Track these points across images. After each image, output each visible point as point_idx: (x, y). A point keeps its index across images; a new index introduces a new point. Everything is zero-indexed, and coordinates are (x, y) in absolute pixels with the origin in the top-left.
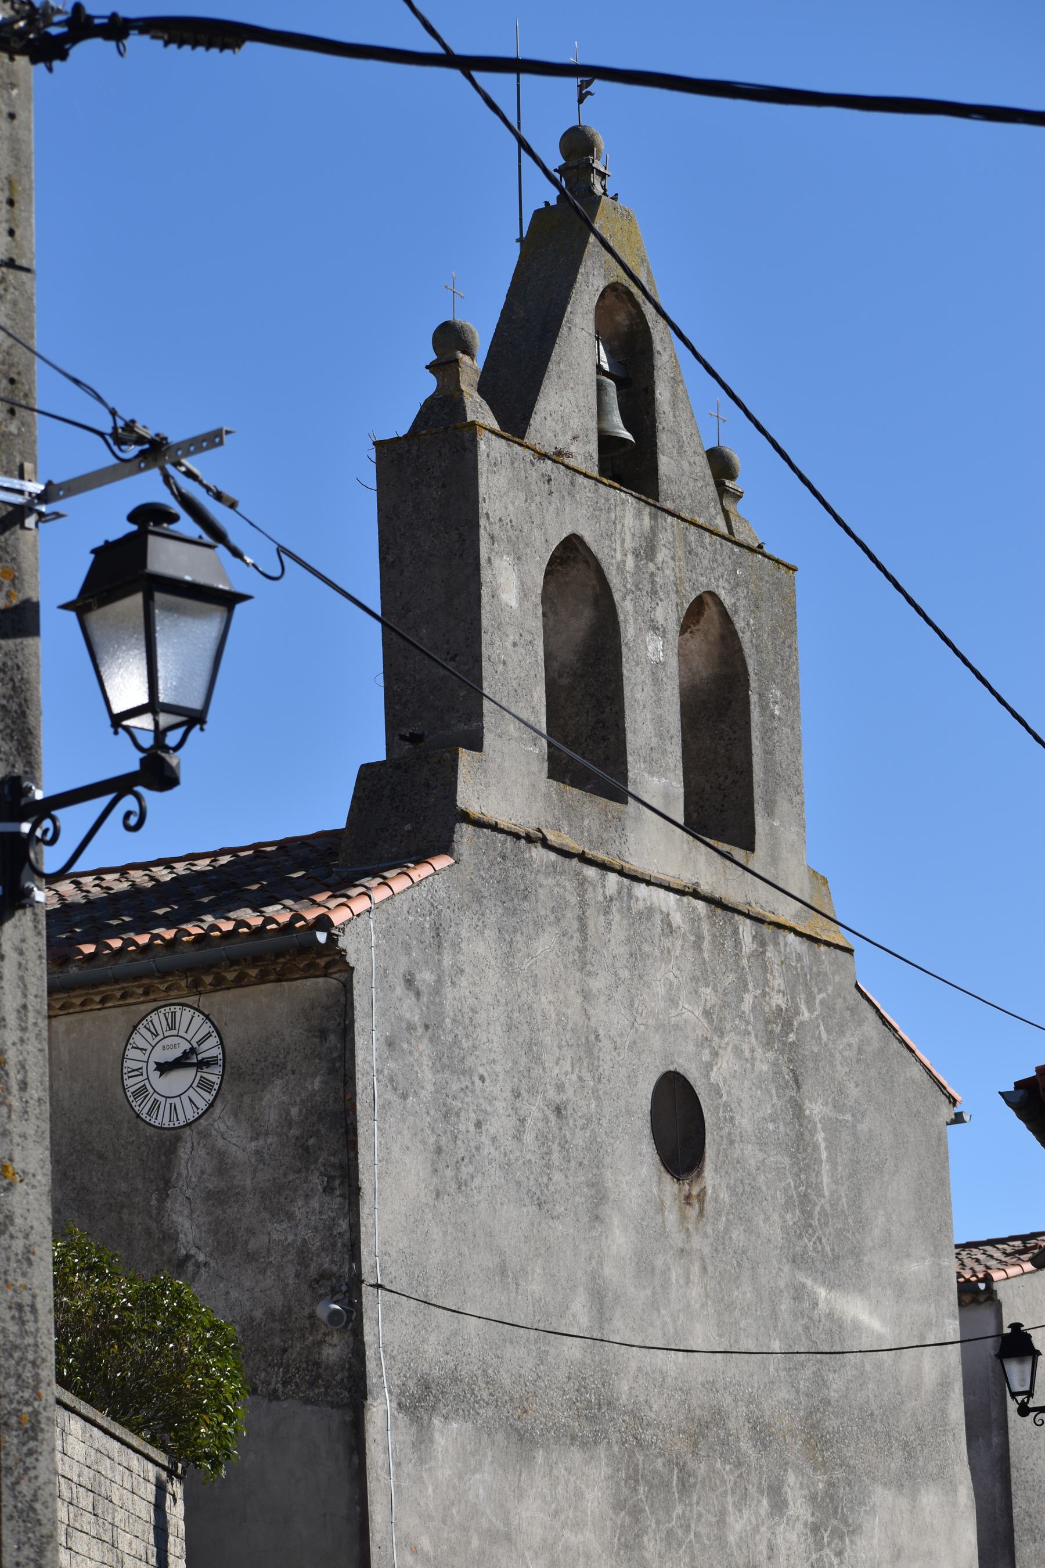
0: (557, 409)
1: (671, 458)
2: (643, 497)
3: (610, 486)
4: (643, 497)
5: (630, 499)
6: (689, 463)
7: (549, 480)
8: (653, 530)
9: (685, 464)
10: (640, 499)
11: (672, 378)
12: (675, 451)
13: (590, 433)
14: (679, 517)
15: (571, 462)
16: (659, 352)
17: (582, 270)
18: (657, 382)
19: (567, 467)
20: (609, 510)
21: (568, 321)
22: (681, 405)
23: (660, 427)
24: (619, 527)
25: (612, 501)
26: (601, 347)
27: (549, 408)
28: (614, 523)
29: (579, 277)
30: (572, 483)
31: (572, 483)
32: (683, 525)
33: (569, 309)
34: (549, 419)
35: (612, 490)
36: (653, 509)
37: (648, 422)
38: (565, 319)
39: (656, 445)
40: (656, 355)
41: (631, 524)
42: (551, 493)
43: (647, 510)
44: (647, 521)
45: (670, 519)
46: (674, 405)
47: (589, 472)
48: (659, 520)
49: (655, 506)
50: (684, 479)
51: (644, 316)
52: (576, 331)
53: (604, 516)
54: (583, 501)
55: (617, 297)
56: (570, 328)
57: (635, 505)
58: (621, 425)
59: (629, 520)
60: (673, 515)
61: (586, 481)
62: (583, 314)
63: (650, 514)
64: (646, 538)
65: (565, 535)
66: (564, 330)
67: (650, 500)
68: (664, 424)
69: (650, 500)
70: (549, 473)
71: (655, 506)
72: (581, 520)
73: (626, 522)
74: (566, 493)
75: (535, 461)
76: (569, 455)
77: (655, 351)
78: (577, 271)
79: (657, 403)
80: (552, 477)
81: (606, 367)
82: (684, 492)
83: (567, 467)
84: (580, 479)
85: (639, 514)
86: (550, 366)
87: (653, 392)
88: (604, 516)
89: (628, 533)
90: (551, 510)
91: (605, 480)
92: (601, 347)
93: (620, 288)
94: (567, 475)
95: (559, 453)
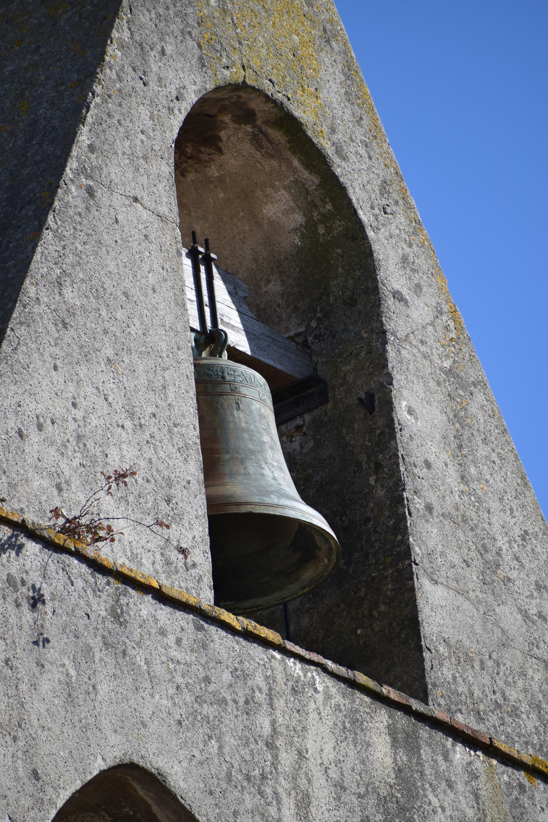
0: (59, 409)
1: (462, 593)
2: (362, 678)
3: (248, 636)
4: (362, 678)
5: (322, 682)
6: (526, 616)
7: (36, 601)
8: (406, 778)
9: (509, 617)
10: (353, 684)
11: (449, 372)
12: (473, 577)
13: (177, 492)
14: (490, 750)
15: (105, 552)
16: (398, 296)
17: (120, 32)
18: (399, 379)
19: (97, 566)
20: (249, 705)
21: (82, 171)
22: (482, 451)
23: (417, 504)
24: (287, 759)
25: (259, 680)
26: (219, 284)
27: (31, 407)
28: (270, 745)
29: (113, 52)
30: (117, 615)
31: (117, 615)
32: (507, 775)
33: (84, 136)
34: (34, 437)
35: (256, 650)
36: (402, 720)
37: (380, 493)
38: (72, 164)
39: (407, 553)
40: (390, 303)
41: (329, 754)
42: (41, 641)
43: (382, 717)
44: (382, 752)
45: (460, 753)
46: (460, 448)
47: (174, 586)
48: (425, 752)
49: (407, 710)
50: (511, 659)
51: (343, 190)
52: (112, 202)
53: (232, 721)
54: (158, 669)
55: (257, 140)
56: (90, 192)
57: (338, 699)
58: (292, 490)
59: (321, 739)
60: (471, 741)
61: (164, 613)
62: (132, 157)
63: (392, 731)
64: (383, 801)
65: (98, 766)
66: (70, 194)
67: (385, 690)
68: (433, 498)
69: (385, 690)
70: (34, 578)
71: (407, 710)
72: (153, 726)
73: (311, 746)
74: (96, 643)
75: (103, 649)
76: (97, 532)
77: (385, 291)
78: (104, 37)
79: (402, 438)
80: (46, 592)
81: (239, 340)
82: (513, 695)
83: (97, 566)
84: (145, 607)
85: (352, 728)
86: (30, 288)
87: (388, 406)
88: (232, 721)
89: (319, 779)
90: (46, 686)
91: (227, 617)
92: (219, 284)
93: (257, 105)
94: (97, 591)
95: (71, 528)
